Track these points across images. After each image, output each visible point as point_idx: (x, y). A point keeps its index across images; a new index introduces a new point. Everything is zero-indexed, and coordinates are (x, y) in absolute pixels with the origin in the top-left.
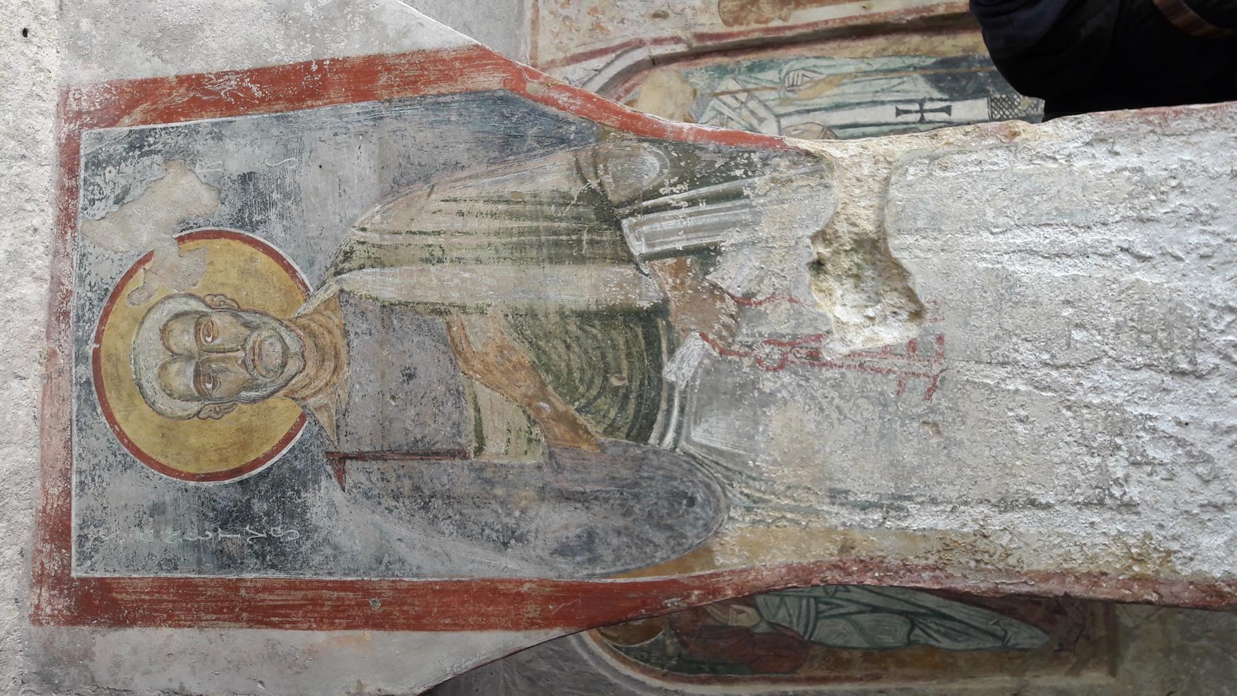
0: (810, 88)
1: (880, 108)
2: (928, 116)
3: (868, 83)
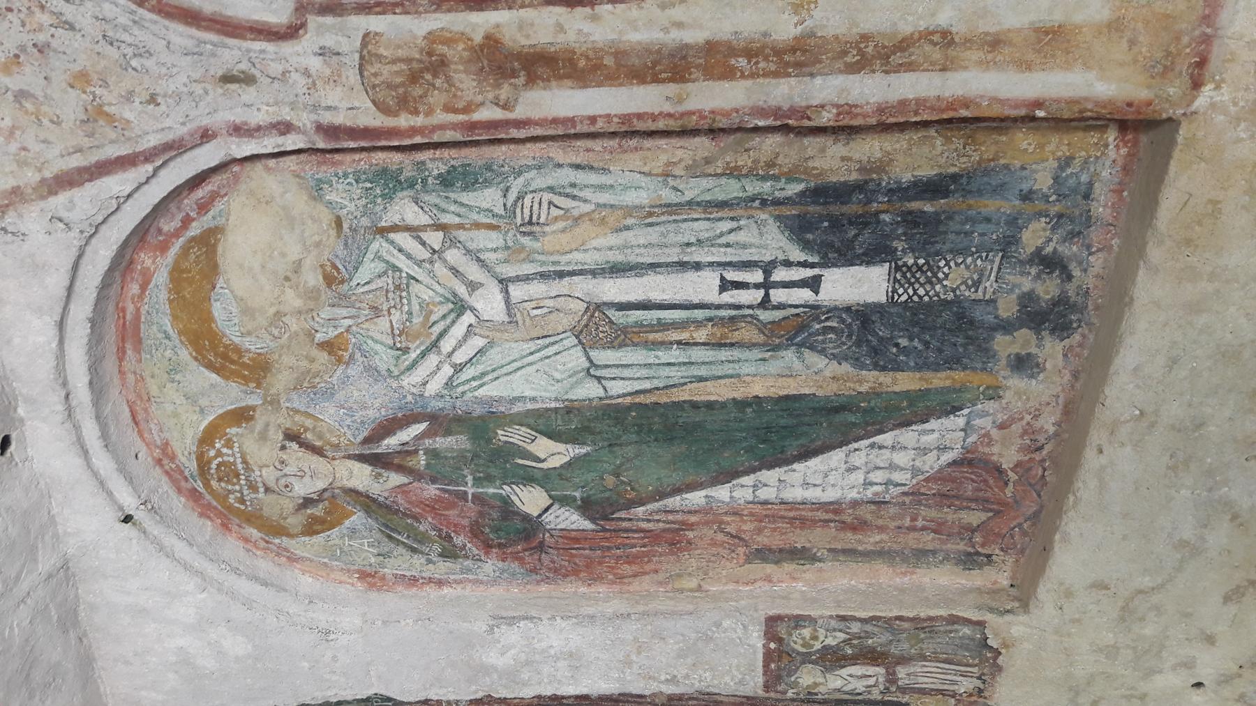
0: (563, 231)
1: (691, 275)
2: (778, 295)
3: (671, 227)
